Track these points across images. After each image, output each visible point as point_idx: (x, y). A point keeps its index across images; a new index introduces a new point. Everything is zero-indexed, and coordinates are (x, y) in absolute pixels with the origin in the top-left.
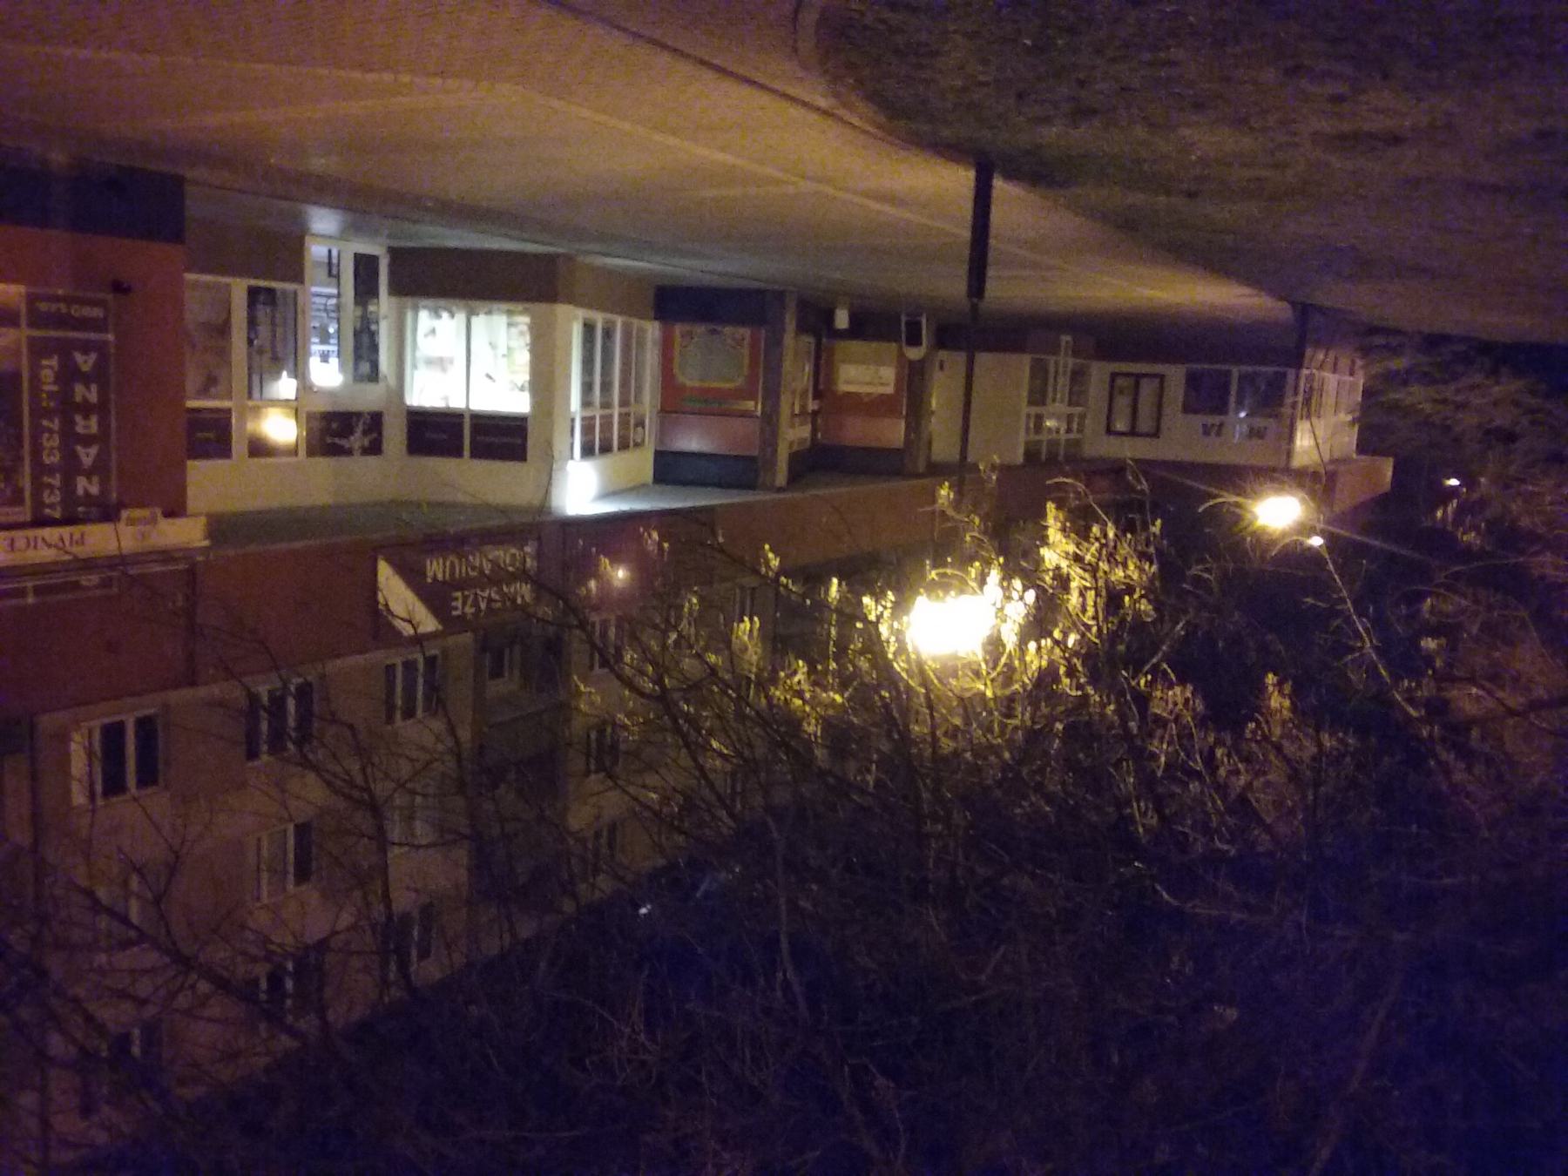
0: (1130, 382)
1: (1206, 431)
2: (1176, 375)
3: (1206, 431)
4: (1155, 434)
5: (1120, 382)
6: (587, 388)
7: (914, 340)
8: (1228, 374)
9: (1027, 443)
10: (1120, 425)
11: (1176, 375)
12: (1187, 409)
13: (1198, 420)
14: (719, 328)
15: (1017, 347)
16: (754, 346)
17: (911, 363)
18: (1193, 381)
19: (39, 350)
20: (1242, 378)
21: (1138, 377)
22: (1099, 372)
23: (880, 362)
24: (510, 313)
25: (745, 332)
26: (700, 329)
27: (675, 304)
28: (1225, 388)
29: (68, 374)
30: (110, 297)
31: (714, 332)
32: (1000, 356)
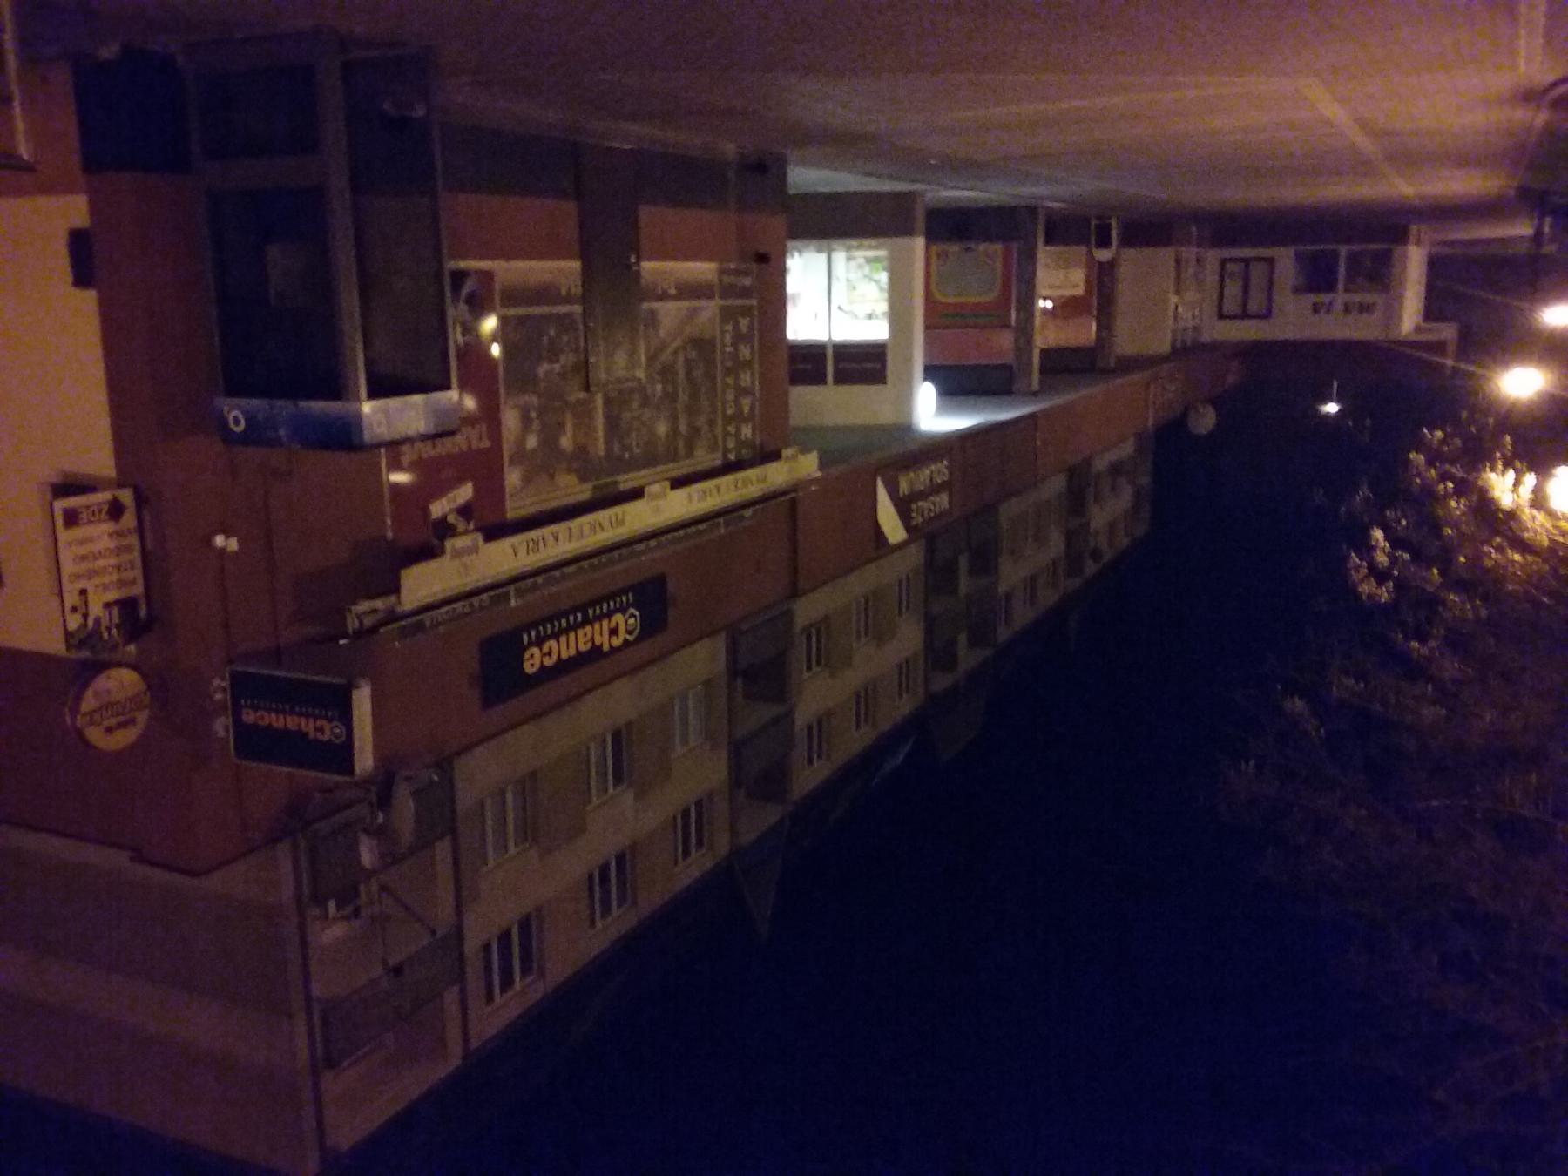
0: (1263, 266)
1: (1316, 309)
2: (1285, 259)
3: (1316, 309)
4: (1266, 315)
5: (1229, 266)
7: (1104, 242)
8: (1335, 255)
9: (1174, 332)
10: (1230, 306)
11: (1285, 259)
12: (1297, 290)
14: (973, 245)
15: (1167, 242)
17: (1101, 264)
19: (727, 315)
21: (1246, 262)
22: (1213, 256)
23: (1068, 265)
24: (848, 249)
25: (998, 247)
26: (954, 248)
27: (951, 226)
28: (1332, 271)
29: (739, 338)
30: (755, 266)
31: (968, 249)
32: (1148, 251)
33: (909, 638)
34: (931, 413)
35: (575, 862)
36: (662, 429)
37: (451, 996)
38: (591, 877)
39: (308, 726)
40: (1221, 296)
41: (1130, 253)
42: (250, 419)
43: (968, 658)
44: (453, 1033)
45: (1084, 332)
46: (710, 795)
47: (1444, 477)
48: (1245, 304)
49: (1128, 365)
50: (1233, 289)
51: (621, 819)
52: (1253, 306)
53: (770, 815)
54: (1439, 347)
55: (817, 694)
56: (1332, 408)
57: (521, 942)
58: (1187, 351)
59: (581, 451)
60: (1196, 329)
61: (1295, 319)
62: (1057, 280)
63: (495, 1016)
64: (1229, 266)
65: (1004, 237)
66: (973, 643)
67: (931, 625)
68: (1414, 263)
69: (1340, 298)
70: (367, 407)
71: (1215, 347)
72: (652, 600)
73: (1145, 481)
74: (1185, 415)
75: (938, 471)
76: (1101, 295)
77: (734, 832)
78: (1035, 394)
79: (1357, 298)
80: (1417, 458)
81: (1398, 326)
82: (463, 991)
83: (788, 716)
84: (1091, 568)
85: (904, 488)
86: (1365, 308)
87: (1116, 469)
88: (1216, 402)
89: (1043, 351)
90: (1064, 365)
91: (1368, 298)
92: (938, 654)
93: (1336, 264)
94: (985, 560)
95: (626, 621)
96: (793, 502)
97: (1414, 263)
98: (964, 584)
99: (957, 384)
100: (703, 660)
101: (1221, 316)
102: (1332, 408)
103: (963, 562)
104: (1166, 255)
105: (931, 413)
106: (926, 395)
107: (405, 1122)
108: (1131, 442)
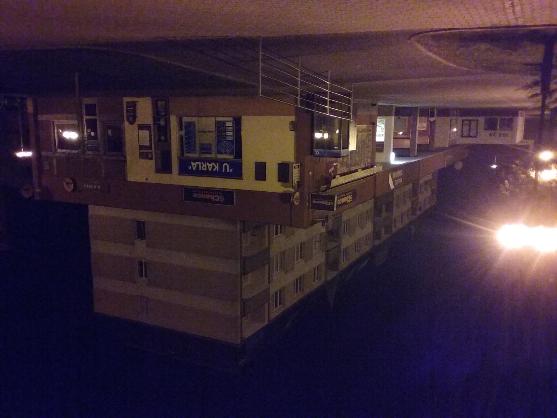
1: (491, 135)
3: (491, 135)
6: (55, 137)
7: (432, 116)
8: (497, 119)
9: (449, 141)
10: (465, 134)
12: (485, 129)
13: (488, 132)
15: (448, 115)
16: (409, 121)
17: (431, 122)
18: (487, 121)
19: (368, 135)
20: (501, 120)
21: (470, 121)
22: (460, 119)
25: (407, 118)
27: (399, 112)
29: (369, 140)
31: (399, 118)
33: (369, 228)
34: (393, 160)
35: (291, 278)
36: (357, 159)
37: (267, 305)
38: (297, 280)
39: (326, 203)
40: (462, 131)
41: (439, 118)
42: (320, 152)
43: (384, 236)
44: (266, 316)
45: (426, 140)
46: (321, 265)
47: (519, 170)
48: (469, 134)
49: (439, 150)
50: (466, 128)
51: (302, 268)
52: (472, 134)
53: (334, 274)
54: (527, 147)
55: (347, 241)
56: (494, 167)
57: (280, 294)
58: (453, 146)
59: (347, 163)
60: (456, 140)
61: (484, 138)
62: (422, 125)
63: (276, 312)
64: (466, 122)
65: (409, 115)
66: (386, 232)
67: (375, 224)
68: (520, 122)
69: (498, 132)
70: (342, 150)
71: (460, 145)
72: (354, 193)
73: (435, 187)
74: (454, 164)
75: (400, 173)
76: (431, 131)
77: (326, 277)
78: (416, 157)
79: (503, 132)
80: (514, 166)
81: (515, 140)
82: (269, 303)
83: (339, 246)
84: (418, 213)
85: (394, 176)
86: (506, 135)
87: (426, 183)
88: (462, 160)
89: (418, 145)
90: (423, 149)
91: (506, 132)
92: (376, 234)
93: (497, 122)
94: (389, 207)
95: (350, 197)
96: (375, 177)
97: (520, 122)
98: (384, 214)
99: (400, 153)
100: (369, 205)
101: (462, 137)
102: (494, 167)
103: (384, 207)
104: (448, 119)
105: (393, 160)
106: (393, 155)
107: (256, 334)
108: (431, 175)
